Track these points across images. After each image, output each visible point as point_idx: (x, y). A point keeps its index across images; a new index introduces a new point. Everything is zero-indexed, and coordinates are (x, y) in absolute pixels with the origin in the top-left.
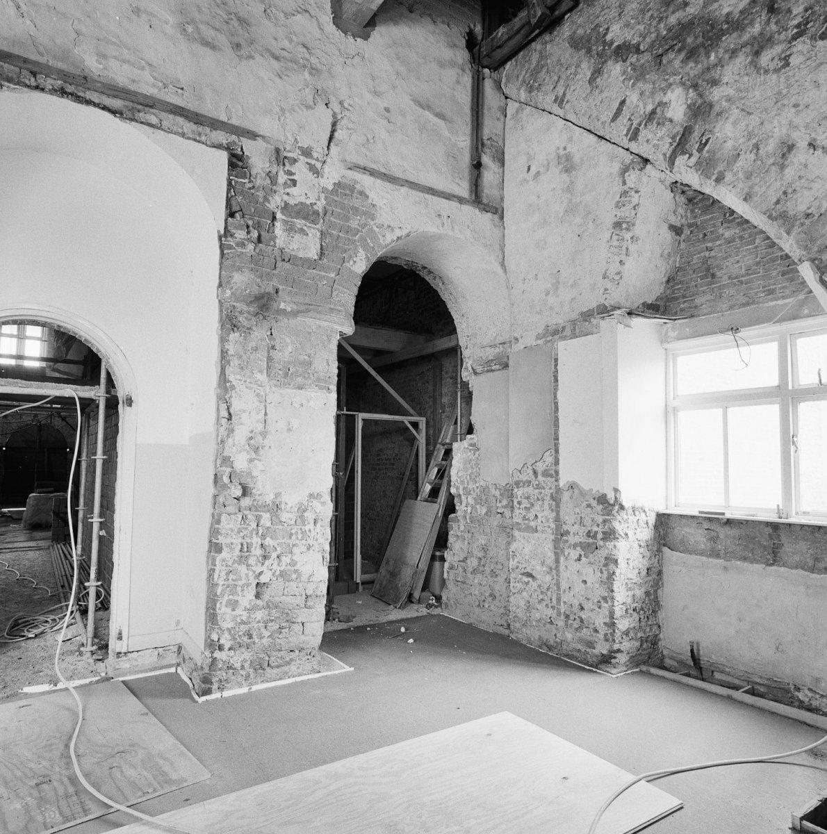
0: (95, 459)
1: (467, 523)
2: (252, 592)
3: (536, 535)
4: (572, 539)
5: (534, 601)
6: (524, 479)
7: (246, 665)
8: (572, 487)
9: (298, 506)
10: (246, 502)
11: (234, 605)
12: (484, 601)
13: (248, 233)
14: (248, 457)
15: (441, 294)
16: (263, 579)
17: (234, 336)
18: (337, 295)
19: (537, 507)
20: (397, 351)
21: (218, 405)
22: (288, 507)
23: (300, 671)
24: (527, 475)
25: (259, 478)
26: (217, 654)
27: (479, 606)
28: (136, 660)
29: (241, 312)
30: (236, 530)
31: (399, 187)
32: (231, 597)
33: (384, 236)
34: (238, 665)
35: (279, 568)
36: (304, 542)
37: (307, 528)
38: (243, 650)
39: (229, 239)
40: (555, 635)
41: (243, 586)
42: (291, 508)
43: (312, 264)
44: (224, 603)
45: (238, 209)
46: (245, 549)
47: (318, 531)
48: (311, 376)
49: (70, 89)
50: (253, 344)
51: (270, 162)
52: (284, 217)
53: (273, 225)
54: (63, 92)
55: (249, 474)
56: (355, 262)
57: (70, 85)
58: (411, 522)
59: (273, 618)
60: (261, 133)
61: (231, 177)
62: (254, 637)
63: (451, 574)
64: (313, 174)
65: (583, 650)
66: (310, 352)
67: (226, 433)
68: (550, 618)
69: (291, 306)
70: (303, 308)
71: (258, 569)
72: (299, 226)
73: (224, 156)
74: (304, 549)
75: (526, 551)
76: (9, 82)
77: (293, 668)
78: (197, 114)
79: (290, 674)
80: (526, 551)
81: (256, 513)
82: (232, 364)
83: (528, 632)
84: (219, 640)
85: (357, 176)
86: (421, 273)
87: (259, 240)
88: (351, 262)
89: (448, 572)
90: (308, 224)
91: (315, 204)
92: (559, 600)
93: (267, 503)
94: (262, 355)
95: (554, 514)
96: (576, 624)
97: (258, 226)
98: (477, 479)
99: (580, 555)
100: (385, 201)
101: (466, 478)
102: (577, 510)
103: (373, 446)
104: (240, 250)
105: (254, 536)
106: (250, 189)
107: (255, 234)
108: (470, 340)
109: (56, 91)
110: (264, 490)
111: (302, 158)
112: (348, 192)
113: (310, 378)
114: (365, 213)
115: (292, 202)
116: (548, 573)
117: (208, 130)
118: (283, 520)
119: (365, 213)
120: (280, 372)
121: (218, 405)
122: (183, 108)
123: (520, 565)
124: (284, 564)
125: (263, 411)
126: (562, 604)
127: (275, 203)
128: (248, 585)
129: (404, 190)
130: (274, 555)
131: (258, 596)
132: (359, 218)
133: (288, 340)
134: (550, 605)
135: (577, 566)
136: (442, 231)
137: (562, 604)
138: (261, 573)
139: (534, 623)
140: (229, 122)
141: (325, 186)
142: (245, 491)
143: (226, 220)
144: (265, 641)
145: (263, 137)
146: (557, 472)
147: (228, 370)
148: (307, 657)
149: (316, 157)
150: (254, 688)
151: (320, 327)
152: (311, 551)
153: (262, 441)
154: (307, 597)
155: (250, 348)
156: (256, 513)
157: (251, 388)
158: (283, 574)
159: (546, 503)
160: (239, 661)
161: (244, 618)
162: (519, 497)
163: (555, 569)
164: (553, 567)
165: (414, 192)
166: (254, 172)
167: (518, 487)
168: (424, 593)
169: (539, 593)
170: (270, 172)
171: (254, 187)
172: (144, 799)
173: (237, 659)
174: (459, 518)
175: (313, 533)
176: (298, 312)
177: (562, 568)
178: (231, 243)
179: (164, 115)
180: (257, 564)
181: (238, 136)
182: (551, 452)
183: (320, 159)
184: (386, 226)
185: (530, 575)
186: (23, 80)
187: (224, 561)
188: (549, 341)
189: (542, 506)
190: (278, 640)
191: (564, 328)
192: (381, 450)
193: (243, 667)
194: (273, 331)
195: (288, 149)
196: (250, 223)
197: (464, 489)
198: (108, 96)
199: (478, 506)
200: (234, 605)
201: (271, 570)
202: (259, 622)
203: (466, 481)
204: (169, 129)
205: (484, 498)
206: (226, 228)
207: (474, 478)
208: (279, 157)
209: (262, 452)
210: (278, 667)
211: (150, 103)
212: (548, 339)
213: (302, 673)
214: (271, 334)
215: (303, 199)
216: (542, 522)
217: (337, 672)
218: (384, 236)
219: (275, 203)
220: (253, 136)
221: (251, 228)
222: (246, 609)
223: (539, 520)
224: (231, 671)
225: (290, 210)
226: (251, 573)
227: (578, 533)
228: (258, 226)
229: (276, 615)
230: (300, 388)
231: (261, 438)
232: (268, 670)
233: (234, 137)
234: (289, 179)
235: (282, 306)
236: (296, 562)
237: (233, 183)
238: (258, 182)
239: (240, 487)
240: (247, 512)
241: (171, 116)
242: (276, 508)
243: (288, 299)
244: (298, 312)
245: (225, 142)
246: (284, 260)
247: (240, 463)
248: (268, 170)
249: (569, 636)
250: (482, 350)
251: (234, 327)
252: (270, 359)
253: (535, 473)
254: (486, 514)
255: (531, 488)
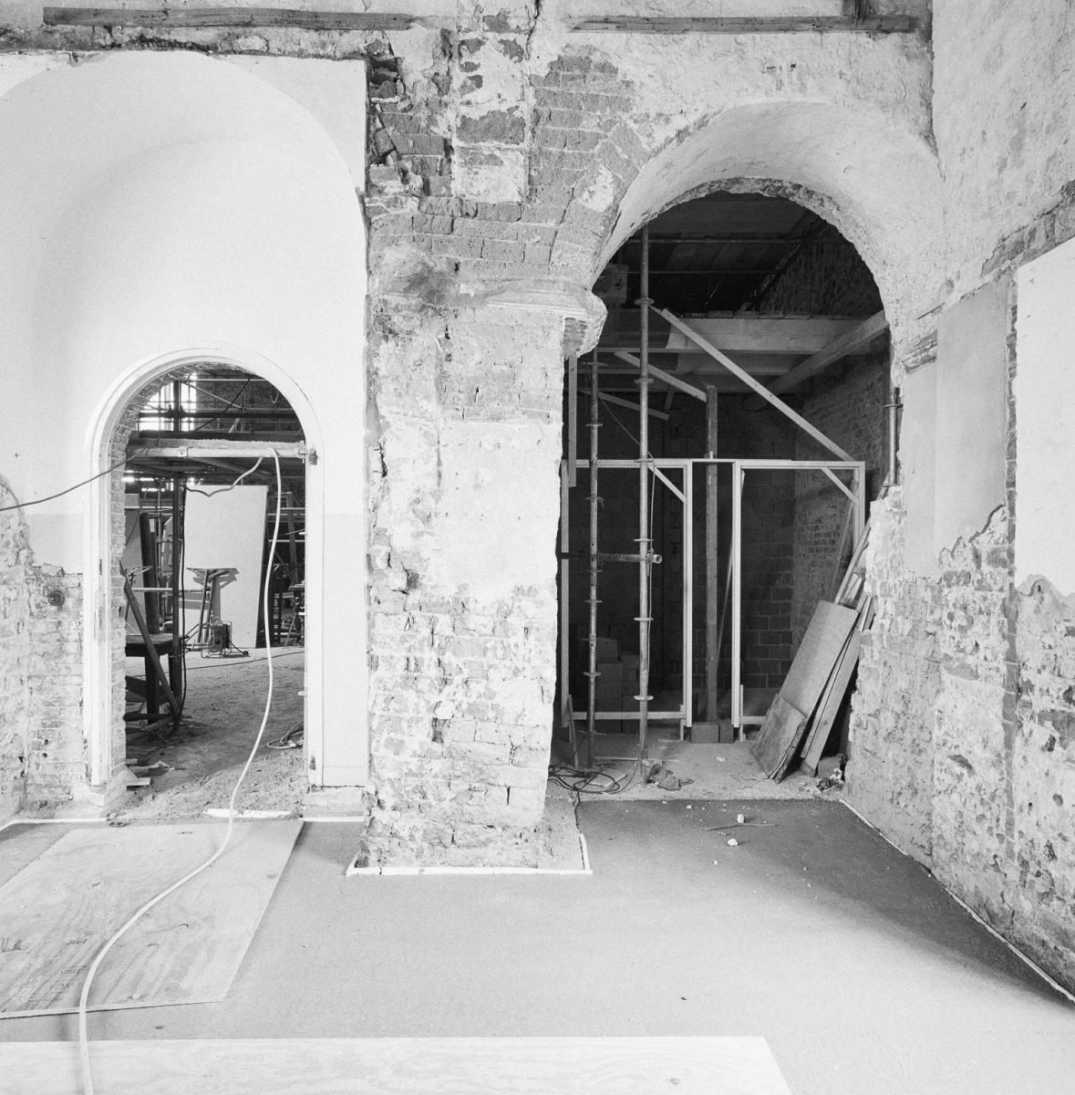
0: (639, 543)
1: (883, 648)
2: (425, 731)
3: (976, 683)
4: (1040, 703)
5: (970, 816)
6: (959, 570)
7: (418, 835)
8: (1039, 588)
9: (496, 606)
10: (415, 596)
11: (398, 747)
12: (900, 794)
13: (405, 181)
14: (413, 529)
15: (842, 230)
16: (442, 714)
17: (387, 348)
18: (559, 257)
19: (978, 628)
20: (818, 352)
21: (367, 453)
22: (479, 607)
23: (503, 859)
24: (963, 563)
25: (431, 561)
26: (377, 812)
27: (892, 800)
28: (335, 798)
29: (396, 309)
30: (398, 639)
31: (682, 36)
32: (392, 734)
33: (649, 135)
34: (405, 834)
35: (466, 700)
36: (507, 662)
37: (512, 641)
38: (414, 812)
39: (375, 198)
40: (1002, 895)
41: (410, 721)
42: (484, 608)
43: (515, 212)
44: (383, 742)
45: (388, 147)
46: (412, 667)
47: (532, 647)
48: (515, 397)
49: (151, 33)
50: (415, 356)
51: (434, 57)
52: (462, 144)
53: (450, 161)
54: (143, 42)
55: (417, 554)
56: (592, 193)
57: (151, 28)
58: (819, 639)
59: (458, 773)
60: (418, 14)
61: (373, 99)
62: (429, 795)
63: (858, 734)
64: (511, 57)
65: (1052, 945)
66: (511, 358)
67: (380, 495)
68: (995, 856)
69: (476, 287)
70: (495, 287)
71: (434, 698)
72: (487, 153)
73: (360, 67)
74: (507, 673)
75: (959, 713)
76: (82, 49)
77: (490, 853)
78: (316, 15)
79: (486, 861)
80: (959, 713)
81: (431, 614)
82: (384, 390)
83: (959, 873)
84: (377, 793)
85: (593, 38)
86: (795, 199)
87: (426, 189)
88: (586, 195)
89: (854, 731)
90: (504, 145)
91: (517, 107)
92: (1010, 824)
93: (446, 600)
94: (430, 372)
95: (1006, 645)
96: (1041, 886)
97: (422, 167)
98: (901, 569)
99: (1053, 740)
100: (650, 70)
101: (886, 566)
102: (1048, 640)
103: (810, 513)
104: (392, 211)
105: (426, 649)
106: (405, 110)
107: (417, 182)
108: (902, 307)
109: (133, 42)
110: (439, 580)
111: (490, 35)
112: (577, 72)
113: (514, 402)
114: (609, 102)
115: (474, 114)
116: (993, 765)
117: (335, 34)
118: (471, 626)
119: (609, 102)
120: (461, 396)
121: (367, 453)
122: (293, 12)
123: (949, 739)
124: (474, 695)
125: (435, 460)
126: (1016, 835)
127: (446, 124)
128: (418, 721)
129: (691, 39)
130: (458, 679)
131: (437, 737)
132: (598, 113)
133: (474, 343)
134: (995, 831)
135: (1045, 760)
136: (778, 98)
137: (1016, 835)
138: (438, 704)
139: (968, 859)
140: (368, 11)
141: (534, 72)
142: (412, 581)
143: (367, 169)
144: (446, 805)
145: (422, 20)
146: (1011, 555)
147: (380, 399)
148: (515, 840)
149: (514, 27)
150: (429, 871)
151: (529, 315)
152: (520, 678)
153: (434, 506)
154: (514, 749)
155: (411, 363)
156: (431, 614)
157: (413, 425)
158: (473, 710)
159: (994, 620)
160: (407, 829)
161: (414, 768)
162: (951, 604)
163: (1003, 759)
164: (1003, 755)
165: (713, 37)
166: (409, 81)
167: (949, 586)
168: (828, 761)
169: (976, 800)
170: (437, 74)
171: (411, 106)
172: (123, 1006)
173: (405, 823)
174: (873, 638)
175: (522, 651)
176: (486, 295)
177: (1017, 760)
178: (379, 204)
179: (271, 32)
180: (430, 691)
181: (381, 29)
182: (1003, 512)
183: (523, 28)
184: (653, 115)
185: (964, 763)
186: (96, 41)
187: (380, 681)
188: (1004, 272)
189: (986, 626)
190: (466, 806)
191: (1032, 234)
192: (819, 520)
193: (412, 838)
194: (449, 331)
195: (465, 26)
196: (408, 165)
197: (883, 585)
198: (197, 27)
199: (900, 619)
200: (398, 747)
201: (453, 701)
202: (436, 776)
203: (885, 571)
204: (279, 50)
205: (908, 604)
206: (368, 182)
207: (896, 565)
208: (448, 46)
209: (434, 521)
210: (468, 847)
211: (248, 22)
212: (1003, 268)
213: (502, 863)
214: (447, 337)
215: (495, 106)
216: (986, 659)
217: (562, 872)
218: (649, 135)
219: (446, 124)
220: (405, 22)
221: (411, 174)
222: (414, 754)
223: (981, 654)
224: (396, 841)
225: (472, 129)
226: (422, 704)
227: (1048, 691)
228: (422, 167)
229: (464, 770)
230: (496, 418)
231: (433, 501)
232: (452, 848)
233: (377, 34)
234: (470, 78)
235: (463, 289)
236: (495, 693)
237: (378, 107)
238: (420, 96)
239: (404, 575)
240: (415, 613)
241: (282, 30)
242: (461, 607)
243: (472, 276)
244: (486, 295)
245: (362, 46)
246: (467, 214)
247: (402, 539)
248: (432, 72)
249: (1027, 906)
250: (921, 321)
251: (390, 333)
252: (442, 377)
253: (977, 557)
254: (911, 634)
255: (970, 588)
